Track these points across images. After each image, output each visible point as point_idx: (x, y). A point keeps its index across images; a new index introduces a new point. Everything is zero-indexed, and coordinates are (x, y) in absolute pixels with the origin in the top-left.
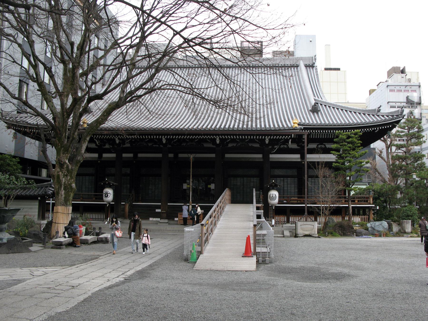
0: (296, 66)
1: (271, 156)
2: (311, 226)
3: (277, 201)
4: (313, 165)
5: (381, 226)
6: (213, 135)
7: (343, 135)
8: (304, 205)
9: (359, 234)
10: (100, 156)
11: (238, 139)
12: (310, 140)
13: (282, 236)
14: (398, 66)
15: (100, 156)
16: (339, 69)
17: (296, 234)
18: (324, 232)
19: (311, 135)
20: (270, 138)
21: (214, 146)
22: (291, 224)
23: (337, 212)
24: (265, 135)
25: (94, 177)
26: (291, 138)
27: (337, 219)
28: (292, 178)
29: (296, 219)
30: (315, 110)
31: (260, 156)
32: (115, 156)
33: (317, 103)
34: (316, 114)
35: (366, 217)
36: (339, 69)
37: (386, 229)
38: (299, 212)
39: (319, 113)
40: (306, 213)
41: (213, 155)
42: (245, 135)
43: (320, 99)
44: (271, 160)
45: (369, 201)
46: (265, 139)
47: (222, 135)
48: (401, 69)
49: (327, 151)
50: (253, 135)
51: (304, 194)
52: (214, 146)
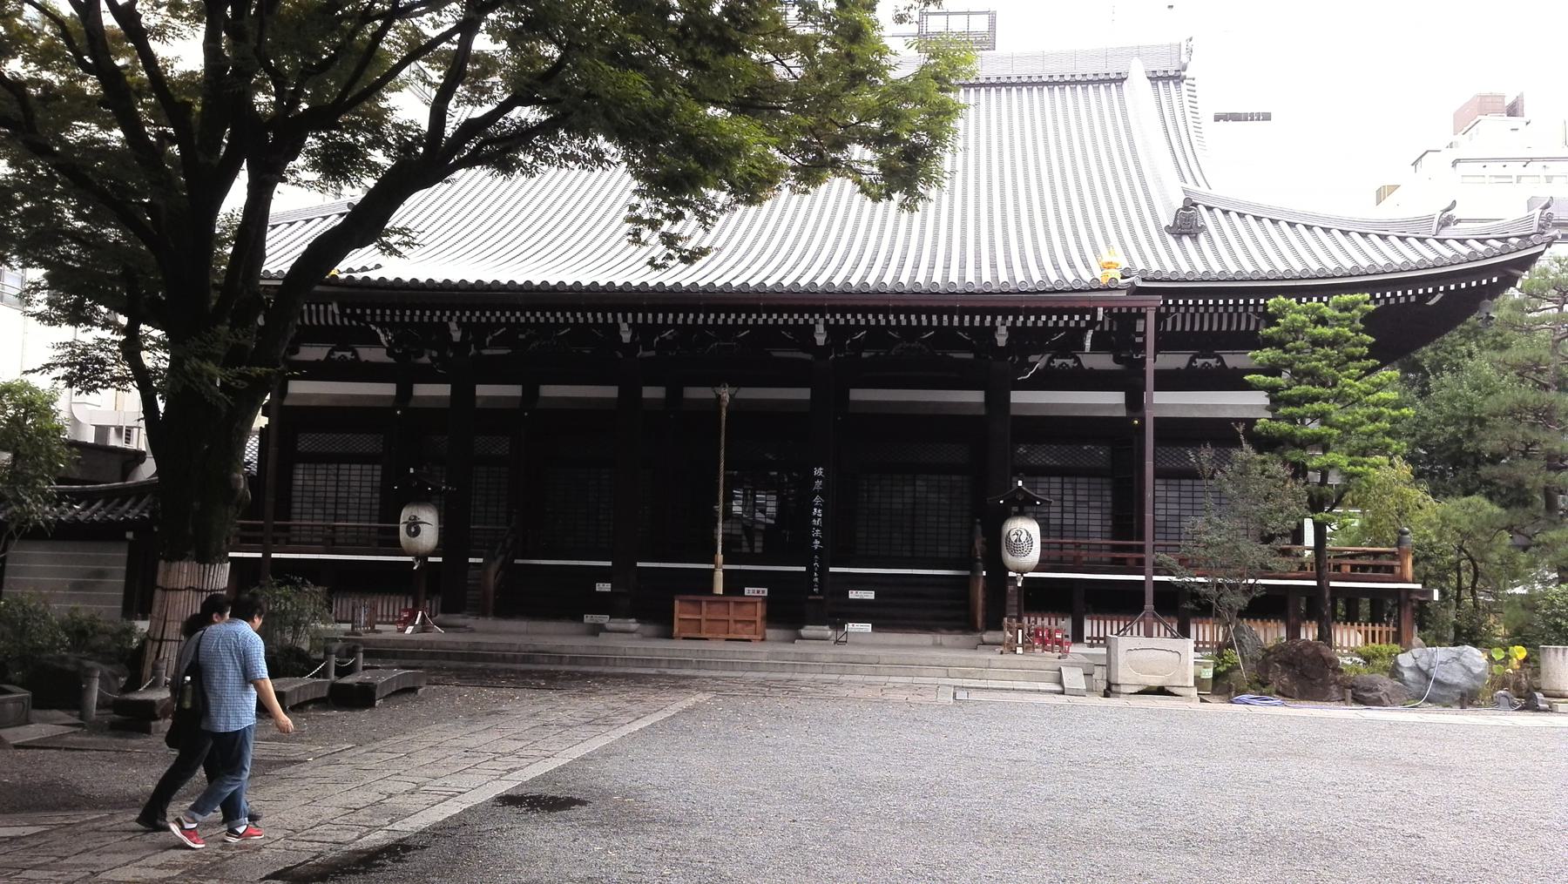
0: (1114, 81)
1: (1018, 397)
2: (1174, 656)
3: (1034, 556)
4: (1179, 432)
5: (1455, 665)
6: (801, 310)
7: (1296, 312)
8: (1142, 578)
9: (1361, 696)
10: (404, 393)
11: (893, 329)
12: (1166, 342)
13: (1058, 688)
14: (1497, 90)
15: (404, 393)
16: (1267, 117)
17: (1109, 685)
18: (1221, 685)
19: (1169, 320)
20: (1014, 322)
21: (808, 357)
22: (1091, 645)
23: (1269, 605)
24: (994, 312)
25: (378, 467)
26: (1093, 323)
27: (1271, 634)
28: (1094, 476)
29: (1108, 627)
30: (1185, 226)
31: (976, 397)
32: (808, 396)
33: (1195, 205)
34: (1186, 240)
35: (1377, 628)
36: (1267, 117)
37: (1477, 677)
38: (1121, 604)
39: (1202, 237)
40: (1149, 605)
41: (804, 394)
42: (918, 311)
43: (1203, 189)
44: (1013, 412)
45: (1398, 570)
46: (994, 328)
47: (833, 310)
48: (1508, 102)
49: (1233, 381)
50: (951, 311)
51: (1141, 537)
52: (808, 357)
